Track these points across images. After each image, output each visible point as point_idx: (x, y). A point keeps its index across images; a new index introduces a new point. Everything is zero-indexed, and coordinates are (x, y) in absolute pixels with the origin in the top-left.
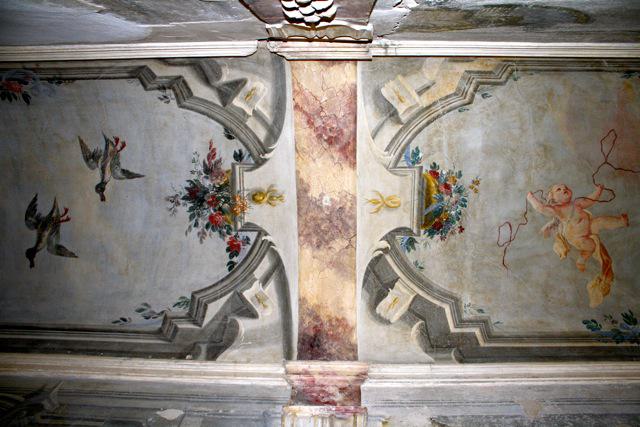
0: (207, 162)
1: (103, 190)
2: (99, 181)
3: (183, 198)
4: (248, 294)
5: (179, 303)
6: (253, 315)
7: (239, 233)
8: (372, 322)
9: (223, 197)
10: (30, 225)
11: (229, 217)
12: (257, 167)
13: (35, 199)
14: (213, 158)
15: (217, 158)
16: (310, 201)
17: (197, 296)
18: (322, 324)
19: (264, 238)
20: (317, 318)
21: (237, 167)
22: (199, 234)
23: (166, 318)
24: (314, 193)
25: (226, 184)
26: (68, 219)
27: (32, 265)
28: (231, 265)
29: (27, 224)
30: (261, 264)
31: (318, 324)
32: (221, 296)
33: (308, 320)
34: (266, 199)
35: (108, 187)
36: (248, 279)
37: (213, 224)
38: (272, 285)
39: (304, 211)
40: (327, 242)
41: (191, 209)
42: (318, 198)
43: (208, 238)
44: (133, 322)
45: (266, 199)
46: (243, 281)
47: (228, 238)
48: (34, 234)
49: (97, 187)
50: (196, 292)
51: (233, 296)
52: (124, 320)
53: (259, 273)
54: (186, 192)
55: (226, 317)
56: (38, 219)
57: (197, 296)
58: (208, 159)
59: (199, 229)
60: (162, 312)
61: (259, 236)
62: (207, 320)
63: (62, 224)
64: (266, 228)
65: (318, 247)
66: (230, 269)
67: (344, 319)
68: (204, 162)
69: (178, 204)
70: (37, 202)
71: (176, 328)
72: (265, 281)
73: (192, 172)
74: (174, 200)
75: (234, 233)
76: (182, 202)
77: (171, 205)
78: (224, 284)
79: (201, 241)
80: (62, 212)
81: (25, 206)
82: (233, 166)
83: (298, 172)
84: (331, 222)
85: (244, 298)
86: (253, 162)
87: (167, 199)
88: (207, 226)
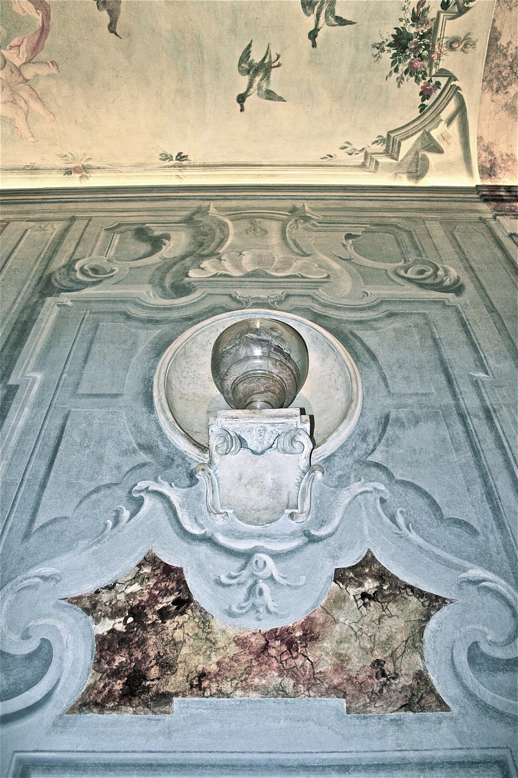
0: (416, 10)
1: (316, 36)
2: (312, 27)
3: (388, 46)
4: (435, 133)
5: (377, 141)
6: (440, 151)
7: (433, 78)
8: (136, 242)
9: (424, 44)
10: (244, 72)
11: (426, 64)
12: (459, 16)
13: (250, 46)
14: (422, 6)
15: (426, 6)
16: (498, 49)
17: (392, 135)
18: (495, 158)
19: (453, 83)
20: (491, 153)
21: (442, 15)
22: (398, 79)
23: (366, 154)
24: (503, 42)
25: (429, 32)
26: (279, 66)
27: (242, 110)
28: (422, 107)
29: (239, 71)
30: (447, 107)
31: (492, 158)
32: (412, 135)
33: (484, 155)
34: (461, 47)
35: (320, 34)
36: (435, 120)
37: (411, 71)
38: (455, 124)
39: (491, 58)
40: (505, 87)
41: (394, 55)
42: (505, 45)
43: (405, 82)
44: (338, 158)
45: (461, 47)
46: (430, 122)
47: (422, 83)
48: (246, 79)
49: (310, 34)
50: (392, 132)
51: (422, 135)
52: (331, 156)
53: (445, 115)
54: (392, 39)
55: (417, 153)
56: (251, 65)
57: (392, 135)
58: (417, 8)
59: (399, 75)
60: (363, 149)
61: (449, 81)
62: (401, 157)
63: (273, 70)
64: (456, 74)
65: (497, 91)
66: (420, 112)
67: (512, 154)
68: (413, 9)
69: (383, 50)
70: (252, 49)
71: (377, 162)
72: (449, 122)
73: (401, 20)
74: (380, 47)
75: (428, 78)
76: (387, 48)
77: (376, 51)
78: (415, 124)
79: (399, 86)
80: (274, 58)
81: (239, 53)
82: (439, 14)
83: (494, 21)
84: (512, 69)
85: (432, 137)
86: (456, 10)
87: (374, 46)
88: (406, 72)
